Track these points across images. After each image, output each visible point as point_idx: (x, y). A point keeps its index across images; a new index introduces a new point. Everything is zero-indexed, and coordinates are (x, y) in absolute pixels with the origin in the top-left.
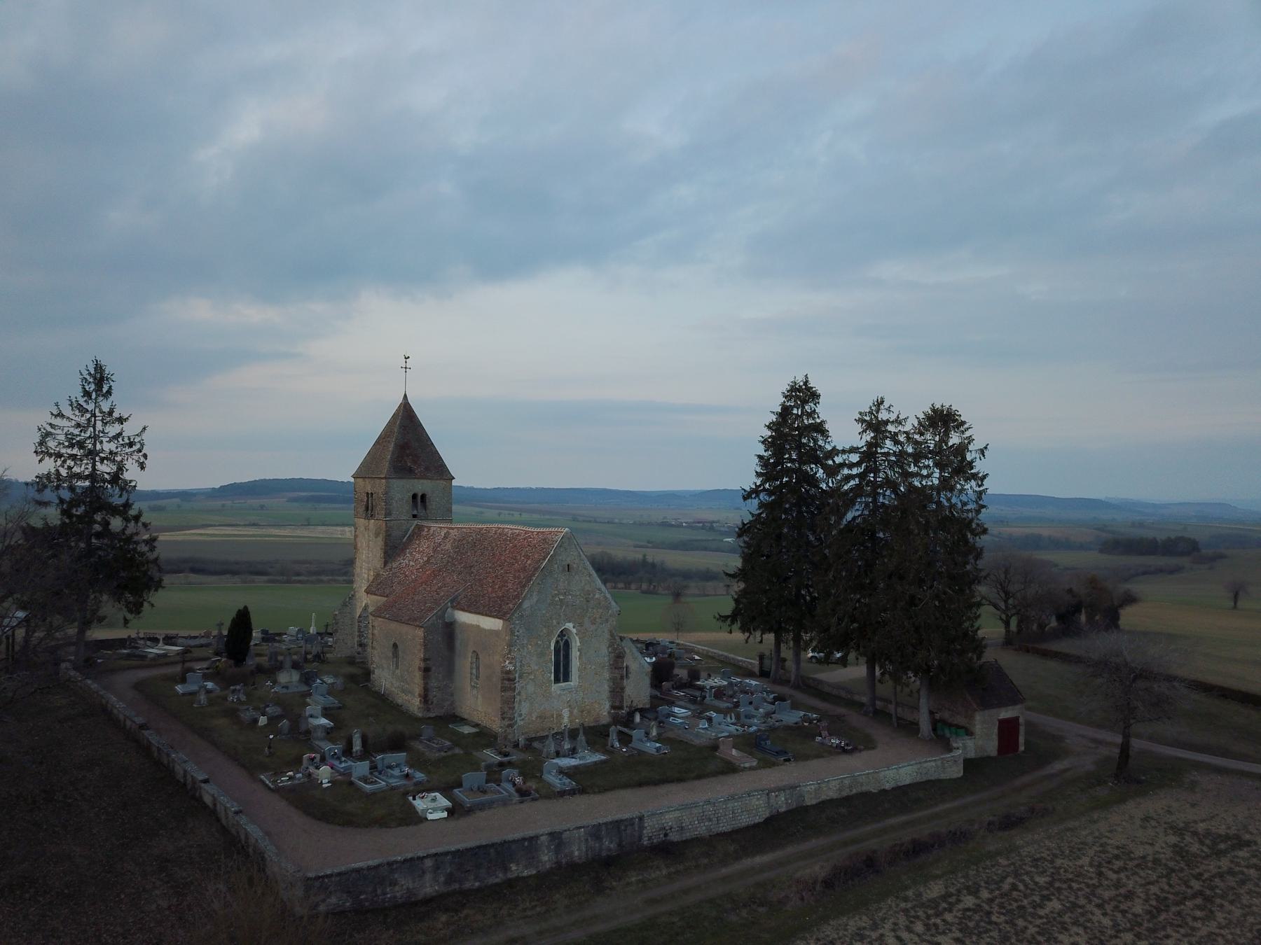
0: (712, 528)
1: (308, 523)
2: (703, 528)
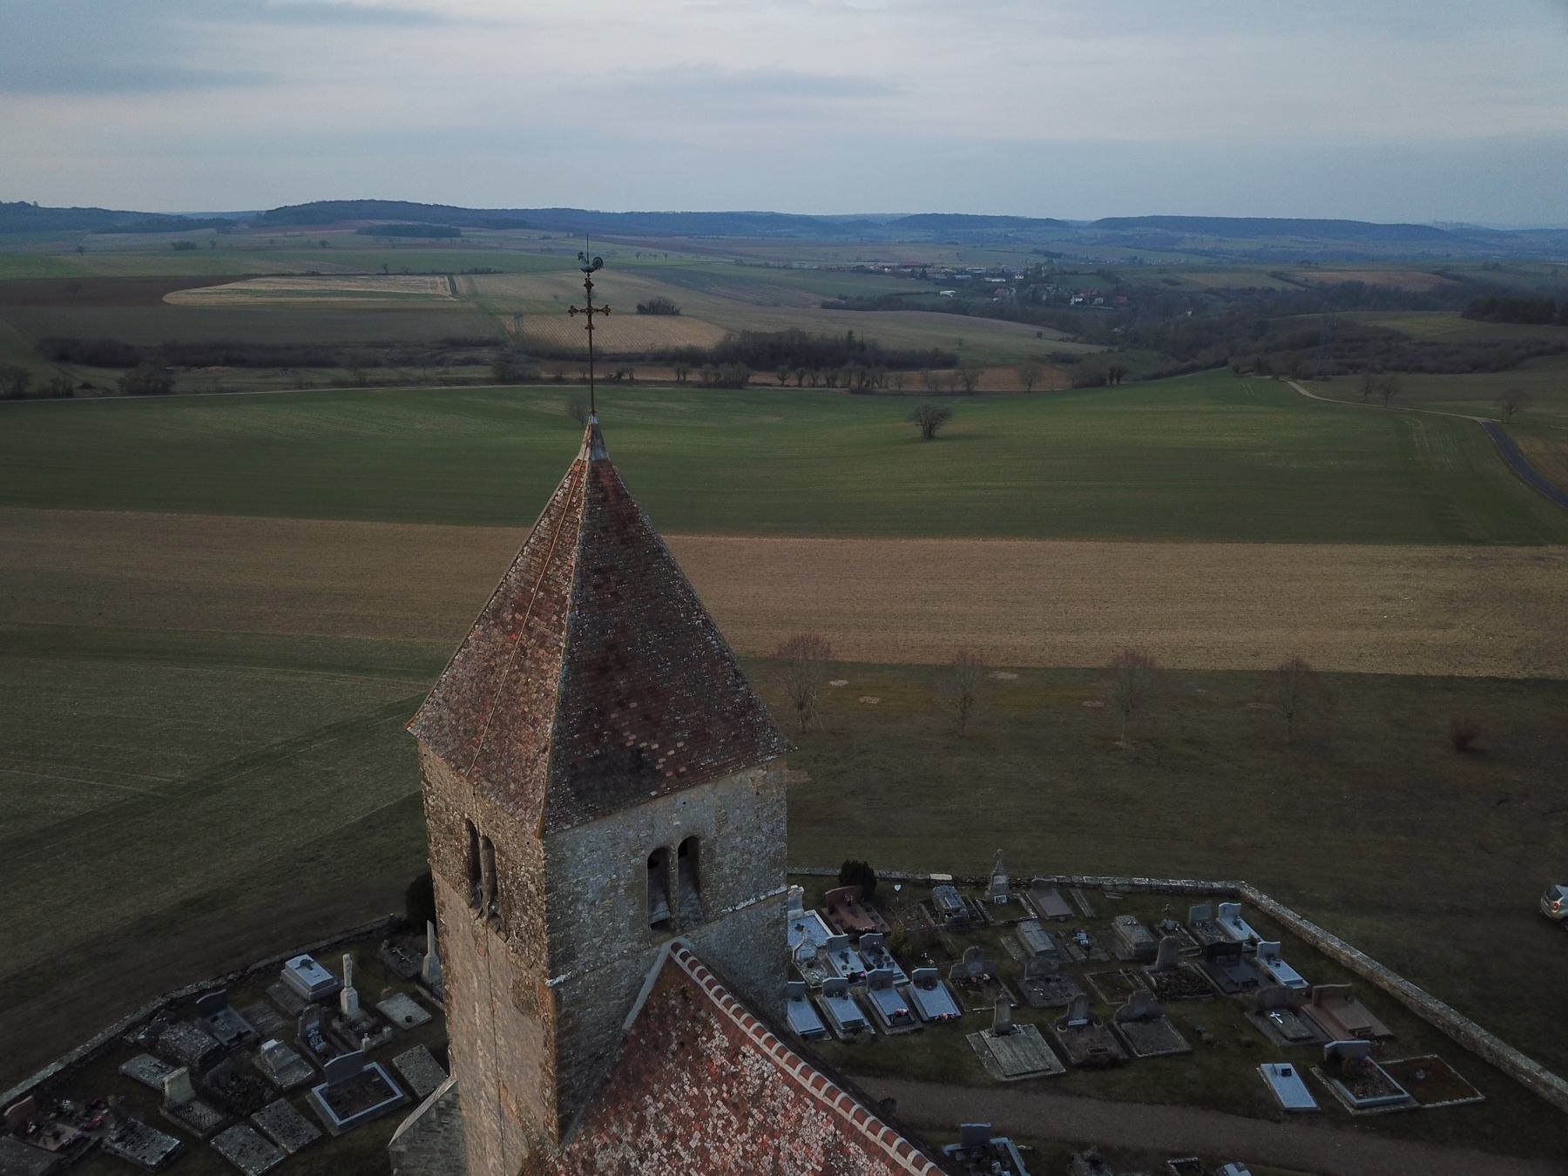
0: (924, 275)
1: (386, 272)
2: (912, 275)
